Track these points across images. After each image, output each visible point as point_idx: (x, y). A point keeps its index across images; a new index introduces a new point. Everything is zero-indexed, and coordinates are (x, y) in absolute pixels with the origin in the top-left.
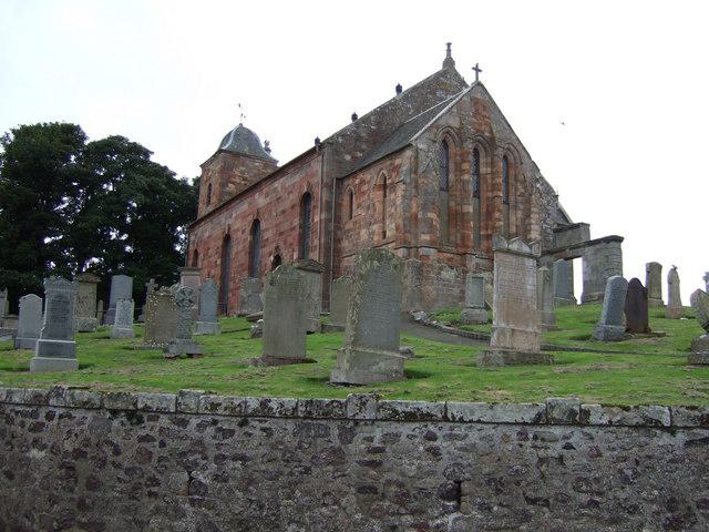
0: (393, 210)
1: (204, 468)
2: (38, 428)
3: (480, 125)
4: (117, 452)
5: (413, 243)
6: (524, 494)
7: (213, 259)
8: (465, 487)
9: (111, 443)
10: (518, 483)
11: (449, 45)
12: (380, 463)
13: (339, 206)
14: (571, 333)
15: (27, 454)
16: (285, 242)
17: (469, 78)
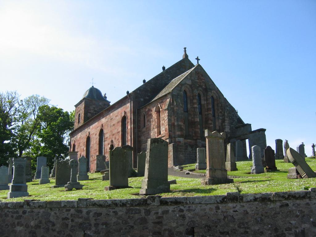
0: (163, 122)
1: (90, 229)
2: (19, 217)
3: (200, 83)
4: (54, 225)
5: (173, 136)
6: (219, 230)
7: (82, 148)
8: (196, 230)
9: (51, 222)
10: (216, 226)
11: (185, 48)
12: (161, 222)
13: (139, 121)
14: (243, 172)
15: (15, 229)
16: (115, 139)
17: (195, 63)
